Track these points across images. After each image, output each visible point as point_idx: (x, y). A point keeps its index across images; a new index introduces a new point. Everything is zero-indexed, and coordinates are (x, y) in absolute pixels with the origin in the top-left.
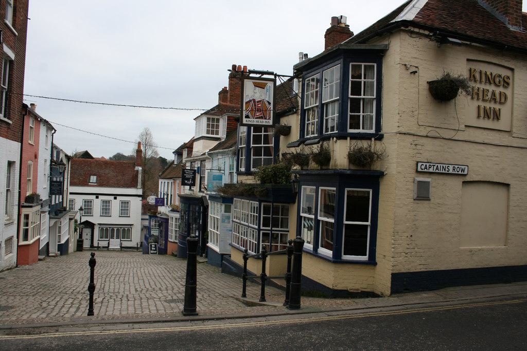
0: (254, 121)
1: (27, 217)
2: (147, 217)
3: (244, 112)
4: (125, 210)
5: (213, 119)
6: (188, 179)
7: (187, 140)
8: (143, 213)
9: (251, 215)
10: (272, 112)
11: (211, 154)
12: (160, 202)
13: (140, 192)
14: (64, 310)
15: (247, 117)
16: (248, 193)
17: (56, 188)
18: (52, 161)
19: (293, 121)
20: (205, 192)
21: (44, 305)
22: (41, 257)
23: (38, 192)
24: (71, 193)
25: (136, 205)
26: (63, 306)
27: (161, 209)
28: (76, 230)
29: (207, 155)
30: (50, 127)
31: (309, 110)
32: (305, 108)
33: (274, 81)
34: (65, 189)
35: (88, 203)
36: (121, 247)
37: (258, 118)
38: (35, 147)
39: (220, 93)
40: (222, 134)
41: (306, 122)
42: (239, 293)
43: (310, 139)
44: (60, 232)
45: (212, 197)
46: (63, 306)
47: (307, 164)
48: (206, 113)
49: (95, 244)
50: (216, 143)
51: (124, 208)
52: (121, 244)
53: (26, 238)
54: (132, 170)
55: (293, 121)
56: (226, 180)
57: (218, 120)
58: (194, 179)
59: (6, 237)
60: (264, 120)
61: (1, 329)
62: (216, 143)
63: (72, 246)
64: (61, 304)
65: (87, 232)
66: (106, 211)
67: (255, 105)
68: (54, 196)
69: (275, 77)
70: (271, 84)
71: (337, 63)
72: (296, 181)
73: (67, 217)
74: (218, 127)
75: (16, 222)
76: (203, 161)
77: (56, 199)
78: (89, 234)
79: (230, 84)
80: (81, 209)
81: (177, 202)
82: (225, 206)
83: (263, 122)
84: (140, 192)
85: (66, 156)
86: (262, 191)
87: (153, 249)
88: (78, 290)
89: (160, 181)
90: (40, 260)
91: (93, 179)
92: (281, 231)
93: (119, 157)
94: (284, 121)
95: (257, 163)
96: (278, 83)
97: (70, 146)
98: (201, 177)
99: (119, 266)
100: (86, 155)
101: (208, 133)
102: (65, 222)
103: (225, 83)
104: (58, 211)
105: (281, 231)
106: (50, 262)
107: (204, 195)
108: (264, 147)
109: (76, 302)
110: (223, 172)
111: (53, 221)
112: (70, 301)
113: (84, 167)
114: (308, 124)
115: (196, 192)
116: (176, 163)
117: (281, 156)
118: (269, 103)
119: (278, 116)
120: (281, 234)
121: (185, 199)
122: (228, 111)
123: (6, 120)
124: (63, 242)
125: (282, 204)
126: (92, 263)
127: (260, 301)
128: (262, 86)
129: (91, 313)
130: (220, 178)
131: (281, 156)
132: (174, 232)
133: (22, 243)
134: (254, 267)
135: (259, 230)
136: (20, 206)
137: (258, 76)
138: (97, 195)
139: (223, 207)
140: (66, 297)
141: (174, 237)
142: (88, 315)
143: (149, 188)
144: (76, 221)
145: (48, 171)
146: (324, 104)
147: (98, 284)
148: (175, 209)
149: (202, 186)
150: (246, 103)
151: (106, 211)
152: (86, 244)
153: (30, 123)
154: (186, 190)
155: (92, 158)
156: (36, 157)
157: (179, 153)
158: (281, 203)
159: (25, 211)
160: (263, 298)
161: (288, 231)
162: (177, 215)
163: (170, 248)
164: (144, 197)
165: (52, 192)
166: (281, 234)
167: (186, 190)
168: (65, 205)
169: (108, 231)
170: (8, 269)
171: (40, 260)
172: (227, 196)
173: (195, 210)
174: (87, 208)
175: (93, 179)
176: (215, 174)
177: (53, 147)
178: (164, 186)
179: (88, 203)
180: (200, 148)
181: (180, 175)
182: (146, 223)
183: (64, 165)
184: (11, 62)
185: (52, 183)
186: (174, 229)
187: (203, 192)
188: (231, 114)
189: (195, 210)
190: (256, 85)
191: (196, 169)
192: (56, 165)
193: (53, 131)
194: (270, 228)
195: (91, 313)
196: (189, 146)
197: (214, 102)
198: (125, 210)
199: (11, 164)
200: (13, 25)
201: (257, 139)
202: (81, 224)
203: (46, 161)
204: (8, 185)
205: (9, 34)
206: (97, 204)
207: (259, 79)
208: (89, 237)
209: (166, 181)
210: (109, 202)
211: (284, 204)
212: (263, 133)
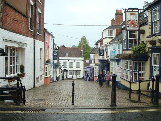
0: (131, 28)
1: (47, 68)
2: (86, 68)
3: (127, 25)
4: (78, 65)
5: (110, 30)
6: (102, 53)
7: (99, 39)
8: (84, 66)
9: (129, 66)
10: (138, 24)
11: (111, 43)
12: (91, 62)
13: (83, 59)
14: (63, 101)
15: (128, 27)
16: (128, 57)
17: (55, 58)
18: (53, 48)
19: (147, 29)
20: (108, 58)
21: (55, 99)
22: (52, 82)
23: (50, 59)
24: (60, 60)
25: (82, 63)
26: (62, 100)
27: (91, 65)
28: (61, 73)
29: (109, 44)
30: (53, 37)
31: (154, 22)
32: (153, 21)
33: (138, 12)
34: (58, 58)
35: (65, 63)
36: (77, 78)
37: (133, 27)
38: (48, 43)
39: (111, 21)
40: (114, 36)
41: (154, 27)
42: (128, 97)
43: (156, 34)
44: (57, 73)
45: (111, 60)
46: (62, 100)
47: (155, 44)
48: (107, 28)
49: (68, 77)
50: (112, 39)
51: (77, 65)
52: (77, 77)
53: (46, 75)
54: (82, 50)
55: (147, 29)
56: (117, 53)
57: (112, 31)
58: (104, 53)
59: (40, 75)
60: (135, 28)
61: (36, 1)
62: (111, 39)
63: (61, 78)
64: (61, 99)
65: (65, 73)
66: (71, 66)
67: (131, 22)
68: (54, 61)
69: (139, 10)
70: (137, 13)
71: (158, 6)
72: (149, 52)
73: (59, 68)
74: (112, 33)
75: (43, 69)
76: (107, 46)
77: (55, 62)
78: (66, 74)
79: (116, 17)
80: (63, 65)
81: (97, 62)
82: (117, 63)
83: (135, 29)
84: (83, 59)
85: (58, 46)
86: (134, 56)
87: (89, 79)
88: (66, 94)
89: (90, 54)
90: (51, 83)
91: (67, 55)
92: (142, 72)
93: (74, 46)
94: (142, 28)
95: (131, 46)
96: (140, 12)
97: (59, 44)
98: (106, 52)
99: (78, 85)
100: (64, 46)
101: (108, 36)
102: (58, 69)
103: (114, 17)
104: (56, 66)
105: (142, 72)
106: (54, 83)
107: (108, 59)
108: (134, 39)
109: (66, 99)
110: (116, 50)
111: (55, 69)
112: (64, 98)
113: (62, 51)
114: (154, 28)
115: (104, 58)
116: (95, 48)
117: (141, 42)
118: (137, 21)
119: (140, 26)
120: (142, 73)
121: (101, 61)
122: (116, 27)
123: (39, 34)
124: (58, 76)
125: (142, 61)
126: (73, 84)
127: (138, 100)
128: (134, 15)
129: (73, 104)
130: (115, 52)
131: (141, 42)
132: (96, 73)
133: (45, 77)
134: (135, 87)
135: (133, 72)
136: (44, 64)
137: (132, 10)
138: (68, 60)
139: (116, 63)
140: (62, 96)
141: (96, 74)
142: (72, 104)
143: (86, 57)
144: (61, 69)
145: (52, 52)
146: (153, 22)
147: (76, 92)
148: (96, 64)
149: (107, 56)
150: (128, 21)
151: (71, 66)
152: (65, 77)
153: (46, 35)
154: (101, 57)
155: (66, 47)
156: (49, 47)
157: (97, 44)
158: (142, 61)
159: (46, 66)
160: (139, 99)
161: (145, 72)
162: (98, 67)
163: (95, 80)
164: (84, 60)
165: (54, 59)
166: (142, 73)
167: (101, 57)
168: (58, 64)
169: (72, 72)
170: (41, 86)
171: (51, 83)
172: (118, 59)
173: (105, 64)
174: (65, 65)
175: (67, 55)
176: (112, 51)
177: (54, 44)
178: (92, 56)
179: (65, 63)
180: (105, 42)
181: (98, 52)
182: (86, 70)
183: (57, 49)
184: (40, 14)
185: (54, 56)
186: (96, 72)
187: (107, 58)
188: (117, 28)
189: (105, 64)
190: (131, 14)
191: (104, 49)
192: (55, 50)
193: (54, 38)
194: (138, 71)
195: (73, 104)
196: (101, 41)
197: (109, 24)
198: (78, 65)
199: (41, 49)
200: (40, 1)
201: (131, 36)
202: (63, 70)
203: (52, 48)
204: (41, 57)
205: (39, 4)
206: (68, 63)
207: (132, 11)
208: (66, 75)
209: (93, 54)
210: (72, 62)
211: (143, 61)
212: (133, 34)
